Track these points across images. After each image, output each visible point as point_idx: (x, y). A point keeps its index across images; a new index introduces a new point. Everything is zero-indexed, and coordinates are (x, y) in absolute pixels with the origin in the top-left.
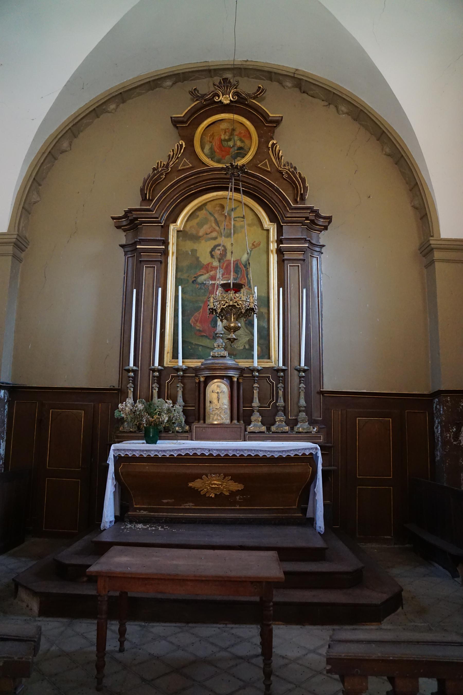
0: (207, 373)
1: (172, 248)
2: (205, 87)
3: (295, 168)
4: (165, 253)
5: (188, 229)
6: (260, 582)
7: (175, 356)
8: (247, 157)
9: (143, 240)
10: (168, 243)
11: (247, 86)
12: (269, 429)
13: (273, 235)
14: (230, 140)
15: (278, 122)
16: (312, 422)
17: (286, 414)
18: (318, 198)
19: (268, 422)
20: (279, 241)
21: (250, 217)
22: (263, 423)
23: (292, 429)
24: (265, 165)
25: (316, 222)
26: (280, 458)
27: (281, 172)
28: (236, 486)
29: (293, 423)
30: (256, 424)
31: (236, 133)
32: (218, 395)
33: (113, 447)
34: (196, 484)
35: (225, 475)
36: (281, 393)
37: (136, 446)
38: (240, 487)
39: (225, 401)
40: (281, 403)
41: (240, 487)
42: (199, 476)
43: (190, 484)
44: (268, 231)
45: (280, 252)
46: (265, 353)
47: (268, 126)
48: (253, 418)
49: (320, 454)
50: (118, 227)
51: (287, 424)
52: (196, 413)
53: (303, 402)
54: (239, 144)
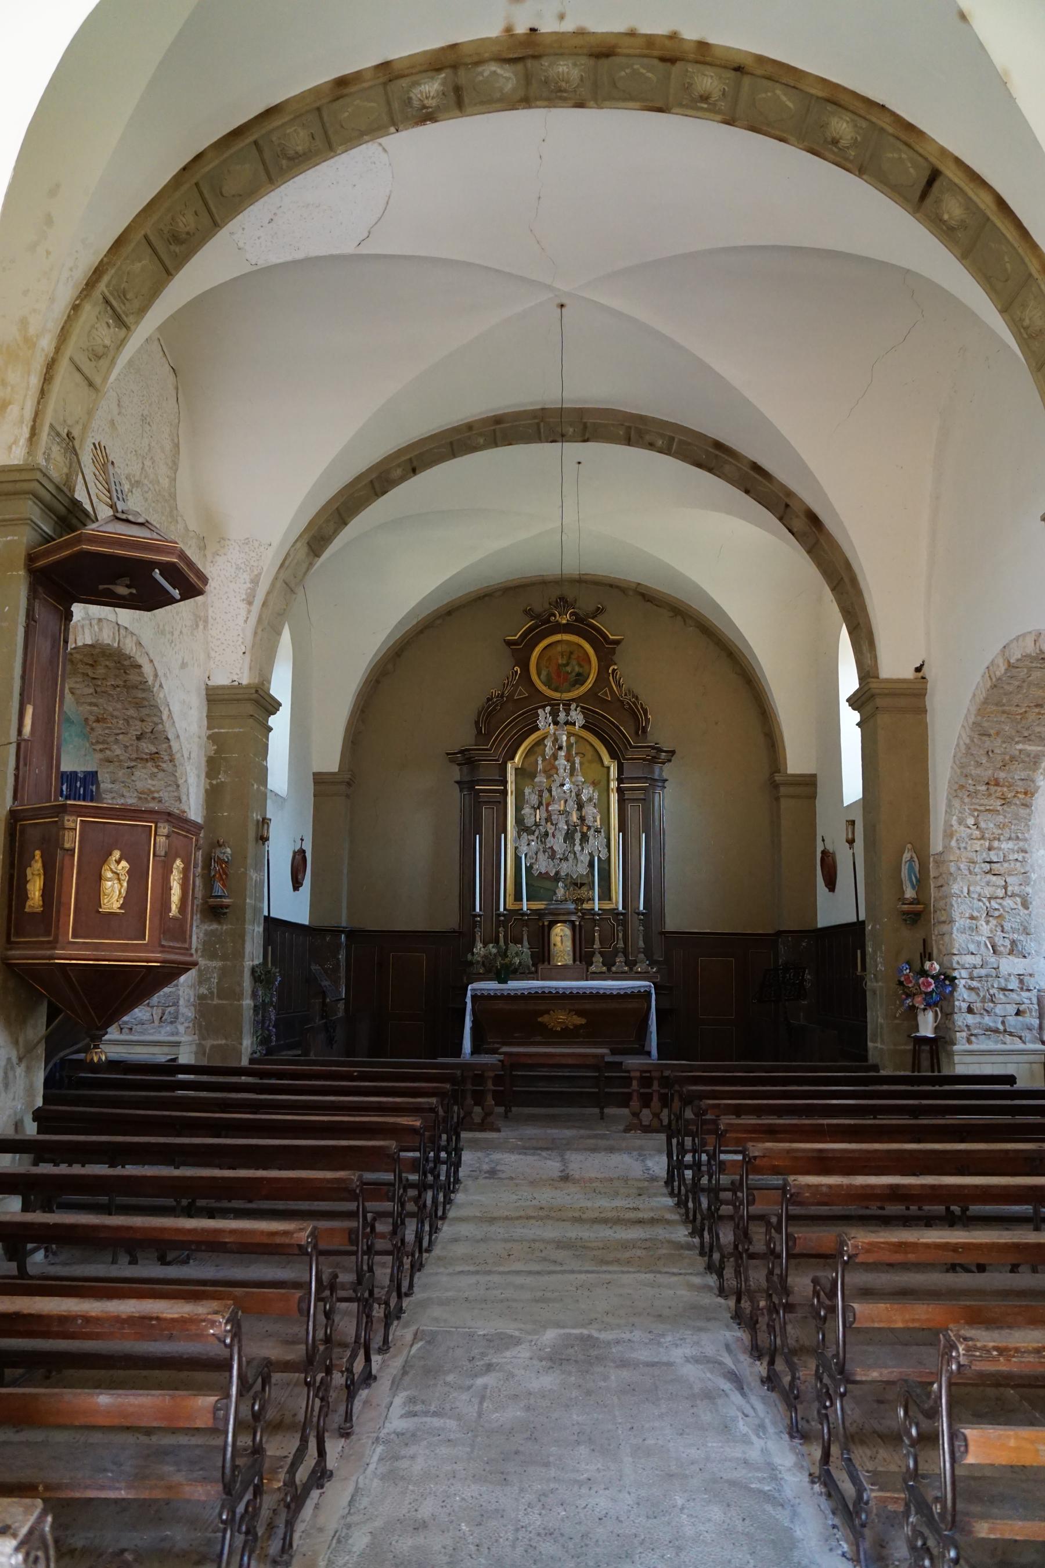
0: (551, 918)
1: (511, 787)
2: (539, 604)
3: (637, 698)
4: (505, 793)
5: (526, 766)
6: (482, 103)
7: (518, 897)
8: (586, 684)
9: (484, 780)
10: (506, 782)
11: (586, 604)
12: (609, 970)
13: (614, 772)
14: (567, 664)
15: (617, 642)
16: (652, 964)
17: (626, 955)
18: (660, 733)
19: (609, 963)
20: (620, 780)
21: (590, 754)
22: (604, 964)
23: (631, 969)
24: (605, 694)
25: (658, 756)
26: (618, 995)
27: (622, 702)
28: (580, 1021)
29: (631, 964)
30: (598, 965)
31: (573, 656)
32: (561, 937)
33: (470, 987)
34: (545, 1019)
35: (570, 1011)
36: (621, 935)
37: (490, 986)
38: (583, 1021)
39: (568, 945)
40: (621, 945)
41: (583, 1021)
42: (547, 1012)
43: (540, 1019)
44: (608, 768)
45: (619, 790)
46: (606, 894)
47: (606, 649)
48: (594, 959)
49: (653, 991)
50: (452, 761)
51: (626, 965)
52: (542, 954)
53: (641, 944)
54: (577, 669)
